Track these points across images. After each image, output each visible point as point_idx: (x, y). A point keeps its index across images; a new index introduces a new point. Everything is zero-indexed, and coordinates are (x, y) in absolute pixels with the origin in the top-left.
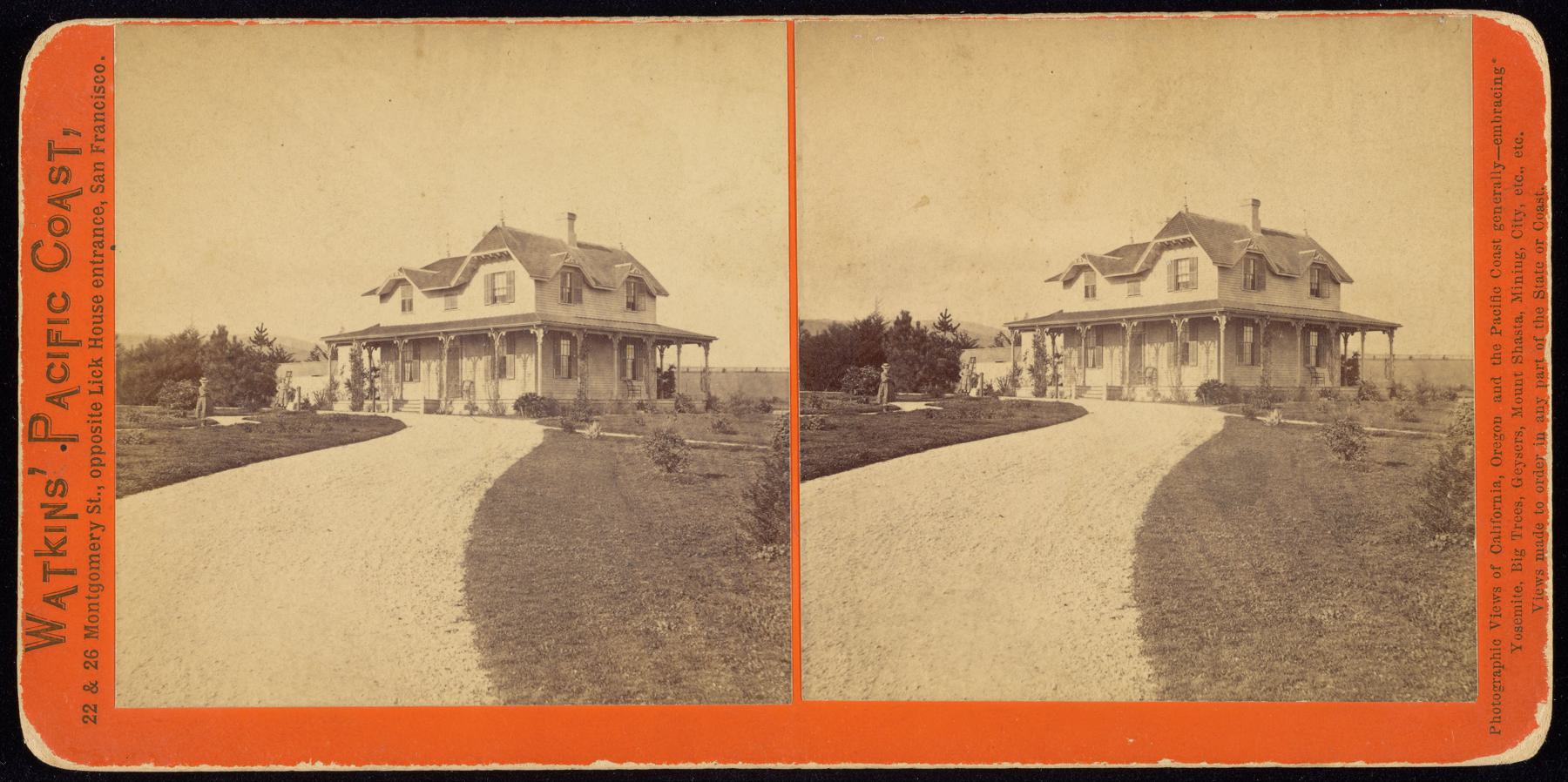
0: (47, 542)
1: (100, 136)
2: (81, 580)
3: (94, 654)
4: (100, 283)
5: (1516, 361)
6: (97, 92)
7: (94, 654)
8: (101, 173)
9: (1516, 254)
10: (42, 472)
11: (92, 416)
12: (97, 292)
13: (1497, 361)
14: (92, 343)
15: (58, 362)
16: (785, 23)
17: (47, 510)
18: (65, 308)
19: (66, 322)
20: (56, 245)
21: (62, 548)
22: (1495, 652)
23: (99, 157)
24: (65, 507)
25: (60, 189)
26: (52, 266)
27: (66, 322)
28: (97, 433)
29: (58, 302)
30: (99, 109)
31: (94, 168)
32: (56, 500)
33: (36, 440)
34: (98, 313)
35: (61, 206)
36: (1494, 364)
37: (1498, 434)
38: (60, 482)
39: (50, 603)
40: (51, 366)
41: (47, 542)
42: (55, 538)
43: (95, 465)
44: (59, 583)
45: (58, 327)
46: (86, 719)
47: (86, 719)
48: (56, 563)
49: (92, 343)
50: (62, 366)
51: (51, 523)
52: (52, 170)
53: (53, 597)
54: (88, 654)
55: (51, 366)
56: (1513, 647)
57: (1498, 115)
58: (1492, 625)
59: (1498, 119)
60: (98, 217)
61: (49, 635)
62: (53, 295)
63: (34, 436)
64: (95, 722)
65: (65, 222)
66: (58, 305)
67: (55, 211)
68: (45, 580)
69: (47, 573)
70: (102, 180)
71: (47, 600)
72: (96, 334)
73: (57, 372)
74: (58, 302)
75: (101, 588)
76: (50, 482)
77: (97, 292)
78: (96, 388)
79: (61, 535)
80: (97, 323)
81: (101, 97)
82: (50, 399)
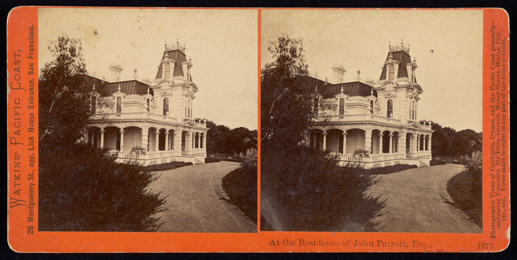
1: (32, 52)
4: (32, 191)
6: (31, 37)
7: (32, 228)
8: (32, 48)
9: (498, 48)
13: (492, 100)
16: (274, 228)
22: (493, 205)
23: (32, 61)
31: (29, 90)
34: (32, 120)
36: (492, 102)
43: (31, 158)
46: (29, 232)
47: (29, 232)
49: (30, 130)
54: (29, 228)
56: (497, 194)
57: (498, 216)
58: (491, 195)
59: (498, 218)
60: (32, 84)
64: (33, 233)
72: (31, 215)
74: (17, 102)
75: (34, 204)
78: (31, 147)
80: (32, 88)
81: (32, 39)
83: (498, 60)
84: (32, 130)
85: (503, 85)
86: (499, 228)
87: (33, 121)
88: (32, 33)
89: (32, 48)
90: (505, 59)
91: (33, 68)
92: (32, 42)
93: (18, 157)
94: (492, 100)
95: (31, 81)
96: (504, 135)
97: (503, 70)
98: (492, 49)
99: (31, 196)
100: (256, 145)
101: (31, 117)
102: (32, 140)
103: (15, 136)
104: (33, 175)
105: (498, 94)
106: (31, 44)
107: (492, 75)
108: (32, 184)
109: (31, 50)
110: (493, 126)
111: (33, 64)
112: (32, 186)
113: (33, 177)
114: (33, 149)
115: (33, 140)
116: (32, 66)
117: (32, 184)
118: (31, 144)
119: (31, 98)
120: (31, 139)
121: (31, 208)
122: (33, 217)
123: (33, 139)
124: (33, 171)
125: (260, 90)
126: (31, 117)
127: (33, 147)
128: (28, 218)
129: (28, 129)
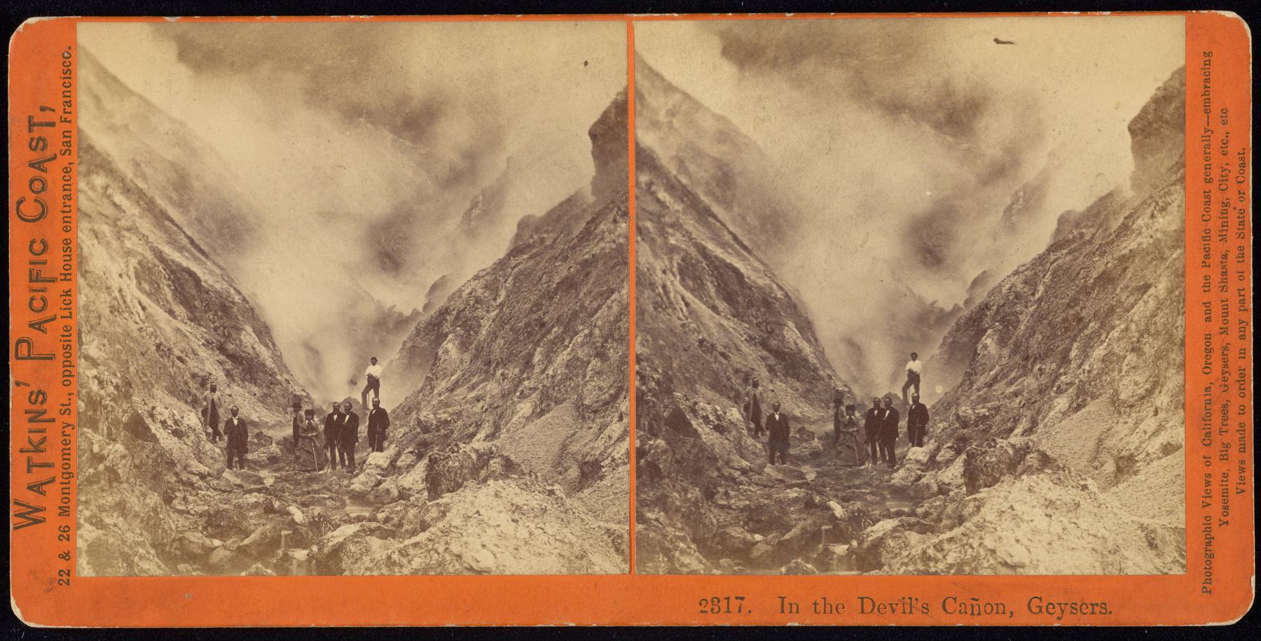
0: (30, 442)
1: (68, 109)
2: (56, 472)
12: (66, 235)
13: (1207, 289)
15: (38, 295)
18: (44, 251)
19: (44, 263)
21: (42, 446)
24: (45, 412)
27: (44, 263)
29: (38, 247)
32: (38, 407)
34: (68, 253)
41: (30, 442)
49: (63, 277)
52: (32, 140)
53: (35, 486)
54: (62, 529)
61: (33, 517)
62: (33, 242)
63: (20, 355)
64: (68, 540)
67: (34, 173)
69: (30, 466)
73: (38, 304)
76: (32, 393)
77: (66, 235)
83: (1225, 228)
84: (68, 277)
85: (834, 607)
86: (1224, 124)
87: (70, 256)
89: (68, 99)
90: (1244, 193)
93: (36, 400)
94: (1207, 289)
95: (66, 168)
96: (1244, 370)
97: (1241, 220)
98: (1206, 349)
101: (66, 68)
102: (67, 298)
103: (33, 334)
104: (70, 404)
107: (1205, 235)
110: (1208, 178)
114: (70, 317)
118: (65, 307)
120: (67, 295)
123: (70, 295)
124: (70, 394)
126: (66, 68)
128: (60, 508)
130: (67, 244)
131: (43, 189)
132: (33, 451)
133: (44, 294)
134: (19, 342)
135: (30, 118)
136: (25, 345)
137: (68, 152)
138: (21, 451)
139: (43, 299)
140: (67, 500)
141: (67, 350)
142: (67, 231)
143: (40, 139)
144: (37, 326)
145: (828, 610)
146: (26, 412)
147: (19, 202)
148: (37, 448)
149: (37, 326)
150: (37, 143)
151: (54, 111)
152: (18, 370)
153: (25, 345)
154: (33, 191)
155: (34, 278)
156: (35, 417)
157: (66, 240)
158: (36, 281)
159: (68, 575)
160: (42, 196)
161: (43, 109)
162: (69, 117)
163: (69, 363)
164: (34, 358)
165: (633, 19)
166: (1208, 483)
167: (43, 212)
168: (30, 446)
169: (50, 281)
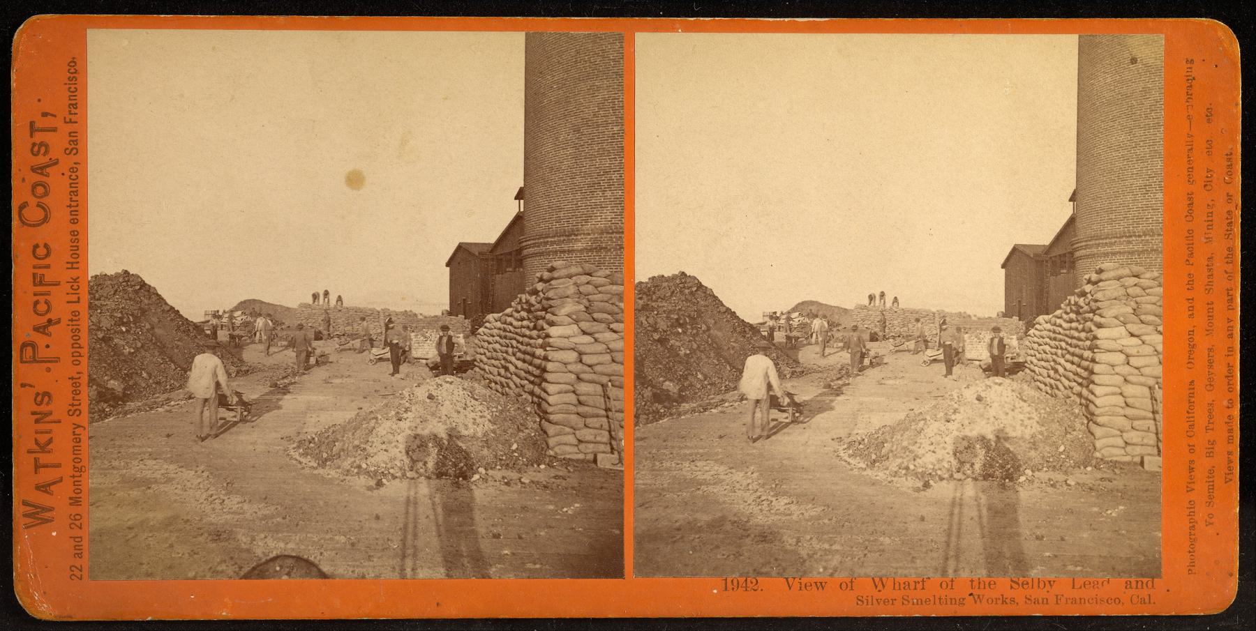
0: (37, 442)
1: (73, 111)
2: (66, 470)
3: (78, 517)
5: (1208, 293)
7: (78, 517)
10: (31, 386)
11: (72, 320)
12: (74, 227)
14: (70, 266)
15: (42, 299)
17: (36, 417)
18: (48, 255)
19: (48, 267)
20: (38, 206)
21: (50, 447)
24: (51, 413)
25: (42, 160)
26: (35, 223)
27: (48, 267)
28: (76, 333)
29: (41, 251)
30: (73, 180)
32: (43, 408)
33: (26, 362)
35: (42, 174)
37: (1191, 344)
38: (47, 394)
39: (40, 490)
40: (36, 303)
41: (37, 442)
42: (43, 439)
44: (46, 475)
45: (40, 271)
46: (73, 526)
47: (73, 577)
48: (44, 458)
49: (70, 266)
50: (46, 303)
51: (40, 427)
52: (34, 144)
53: (43, 486)
55: (36, 303)
60: (74, 174)
61: (40, 515)
62: (36, 246)
63: (24, 359)
64: (81, 528)
65: (45, 187)
66: (42, 252)
67: (37, 178)
68: (36, 473)
69: (37, 466)
70: (76, 145)
71: (38, 488)
73: (42, 307)
74: (41, 251)
76: (38, 394)
77: (74, 227)
78: (74, 298)
79: (48, 436)
82: (36, 329)
84: (75, 265)
88: (77, 287)
89: (74, 102)
91: (76, 141)
92: (72, 89)
99: (77, 450)
100: (637, 372)
105: (1210, 306)
106: (77, 544)
108: (79, 426)
109: (76, 556)
111: (76, 132)
112: (77, 431)
113: (79, 410)
115: (79, 284)
116: (73, 136)
117: (79, 426)
119: (73, 204)
121: (73, 209)
122: (80, 498)
123: (78, 282)
125: (921, 21)
127: (79, 298)
128: (70, 498)
129: (67, 263)
130: (74, 235)
131: (46, 194)
132: (39, 452)
133: (47, 297)
134: (24, 345)
135: (32, 124)
136: (29, 349)
137: (75, 151)
138: (28, 452)
139: (47, 302)
140: (76, 256)
141: (76, 333)
142: (74, 223)
143: (42, 144)
144: (41, 329)
145: (982, 586)
146: (33, 413)
147: (22, 207)
148: (43, 448)
149: (41, 329)
150: (42, 400)
151: (55, 116)
152: (20, 371)
153: (29, 349)
154: (35, 196)
155: (38, 281)
156: (40, 417)
157: (73, 231)
158: (39, 285)
159: (81, 571)
160: (46, 200)
161: (45, 114)
162: (74, 118)
163: (77, 540)
164: (38, 362)
165: (971, 569)
166: (1191, 470)
167: (46, 217)
168: (37, 447)
169: (54, 285)
